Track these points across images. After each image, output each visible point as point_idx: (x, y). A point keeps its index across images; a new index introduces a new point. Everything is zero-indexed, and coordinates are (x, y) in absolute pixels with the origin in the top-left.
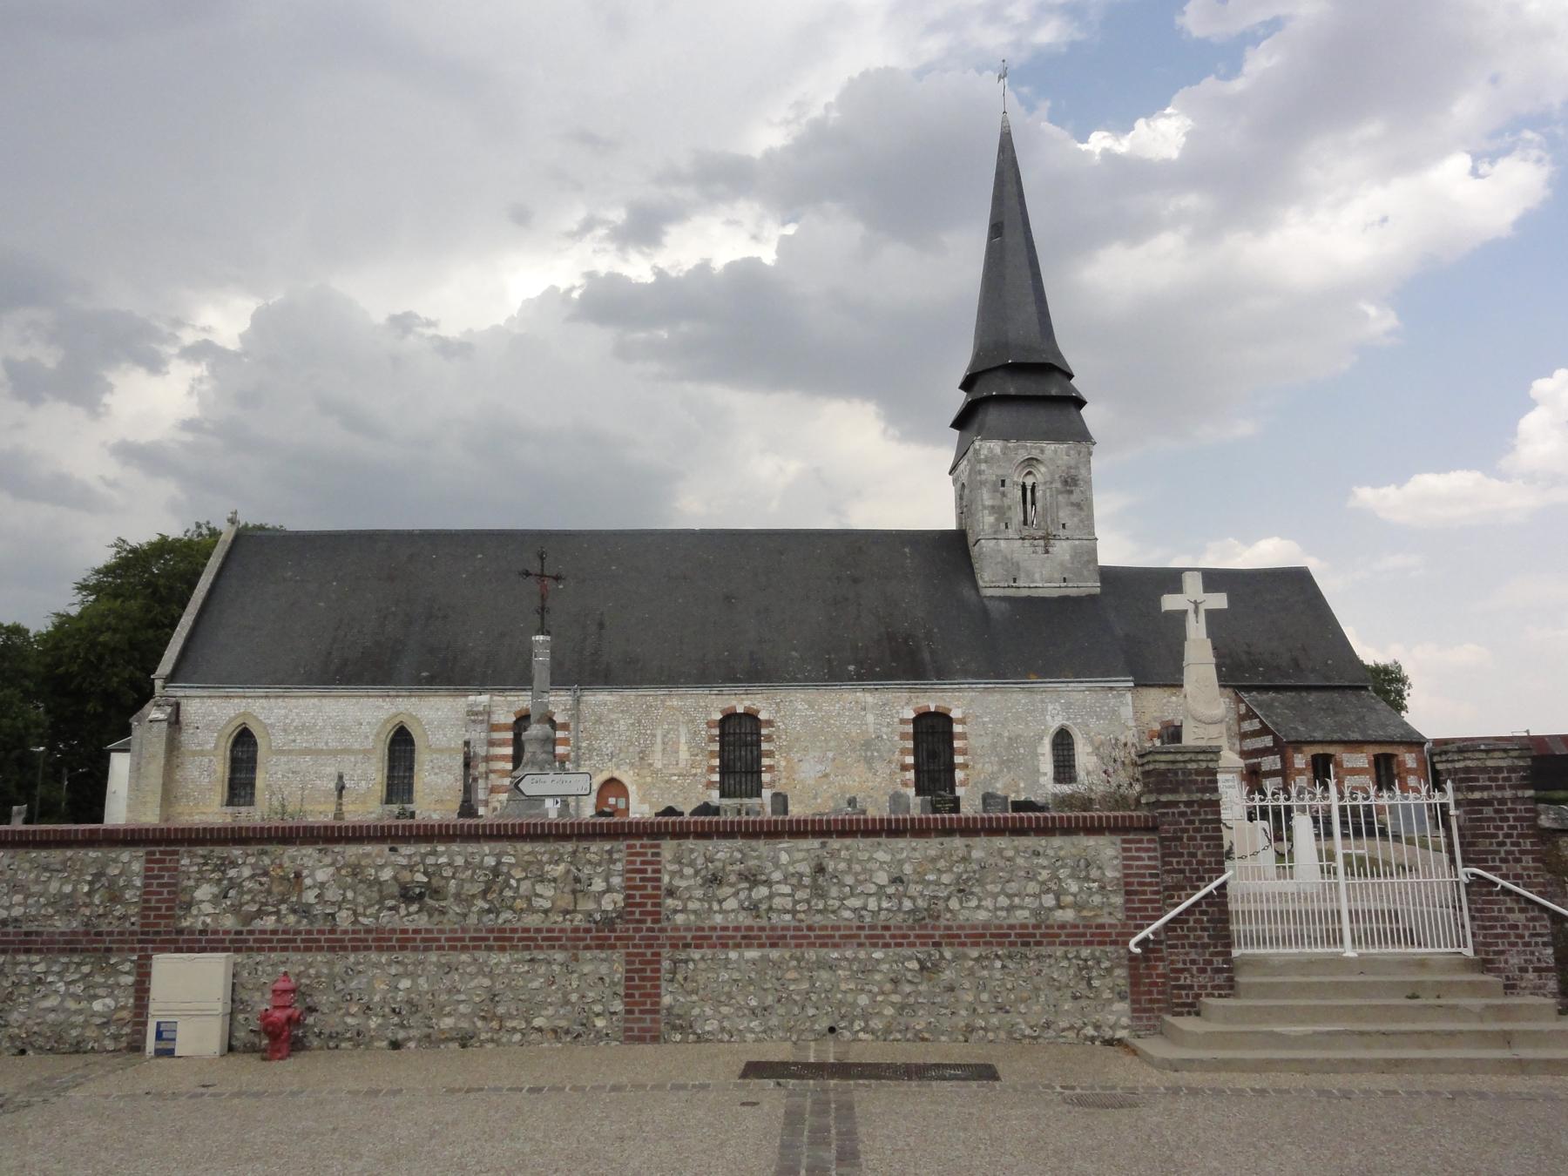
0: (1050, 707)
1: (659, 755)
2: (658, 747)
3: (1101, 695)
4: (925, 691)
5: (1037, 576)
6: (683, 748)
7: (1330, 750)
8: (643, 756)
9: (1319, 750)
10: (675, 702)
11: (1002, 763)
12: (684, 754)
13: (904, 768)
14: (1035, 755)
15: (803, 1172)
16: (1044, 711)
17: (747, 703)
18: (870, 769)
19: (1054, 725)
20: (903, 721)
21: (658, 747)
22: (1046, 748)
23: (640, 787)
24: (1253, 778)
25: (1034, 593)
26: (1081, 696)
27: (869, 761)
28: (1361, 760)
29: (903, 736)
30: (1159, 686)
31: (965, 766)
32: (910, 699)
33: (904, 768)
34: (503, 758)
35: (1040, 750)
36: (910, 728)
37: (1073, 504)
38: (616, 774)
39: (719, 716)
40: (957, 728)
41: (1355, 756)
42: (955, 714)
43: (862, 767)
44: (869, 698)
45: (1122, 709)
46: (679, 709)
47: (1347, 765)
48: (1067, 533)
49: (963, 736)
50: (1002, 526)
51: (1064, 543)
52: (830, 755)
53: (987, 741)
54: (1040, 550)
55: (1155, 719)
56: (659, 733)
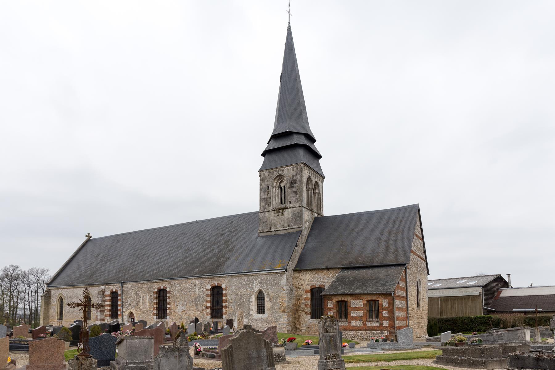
0: (255, 282)
1: (141, 304)
2: (141, 301)
3: (273, 276)
4: (214, 278)
5: (278, 226)
6: (147, 301)
7: (345, 299)
8: (138, 304)
9: (340, 299)
10: (145, 286)
11: (238, 305)
12: (148, 304)
13: (207, 308)
14: (249, 302)
15: (550, 341)
16: (253, 283)
17: (164, 285)
18: (197, 308)
19: (256, 289)
20: (207, 290)
21: (141, 301)
22: (253, 299)
23: (137, 314)
24: (262, 318)
25: (277, 233)
26: (265, 277)
27: (196, 305)
28: (359, 303)
29: (207, 296)
30: (311, 270)
31: (226, 307)
32: (209, 281)
33: (207, 308)
34: (107, 305)
35: (251, 300)
36: (209, 293)
37: (294, 192)
38: (131, 310)
39: (156, 290)
40: (224, 292)
41: (356, 301)
42: (223, 286)
43: (195, 307)
44: (197, 282)
45: (282, 282)
46: (146, 288)
47: (352, 306)
48: (291, 205)
49: (226, 295)
50: (267, 205)
51: (289, 210)
52: (185, 303)
53: (233, 297)
54: (280, 214)
55: (308, 285)
56: (141, 296)
